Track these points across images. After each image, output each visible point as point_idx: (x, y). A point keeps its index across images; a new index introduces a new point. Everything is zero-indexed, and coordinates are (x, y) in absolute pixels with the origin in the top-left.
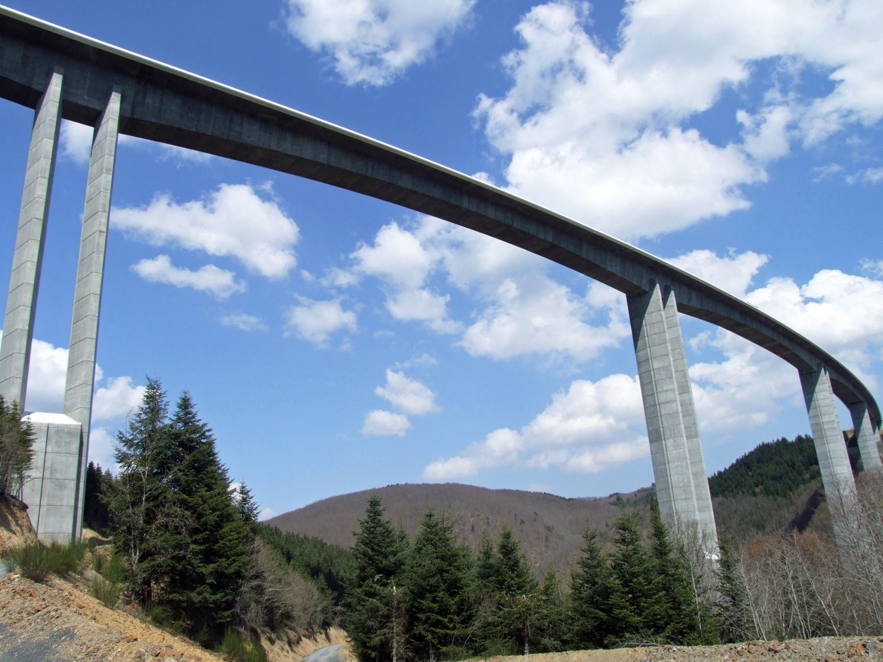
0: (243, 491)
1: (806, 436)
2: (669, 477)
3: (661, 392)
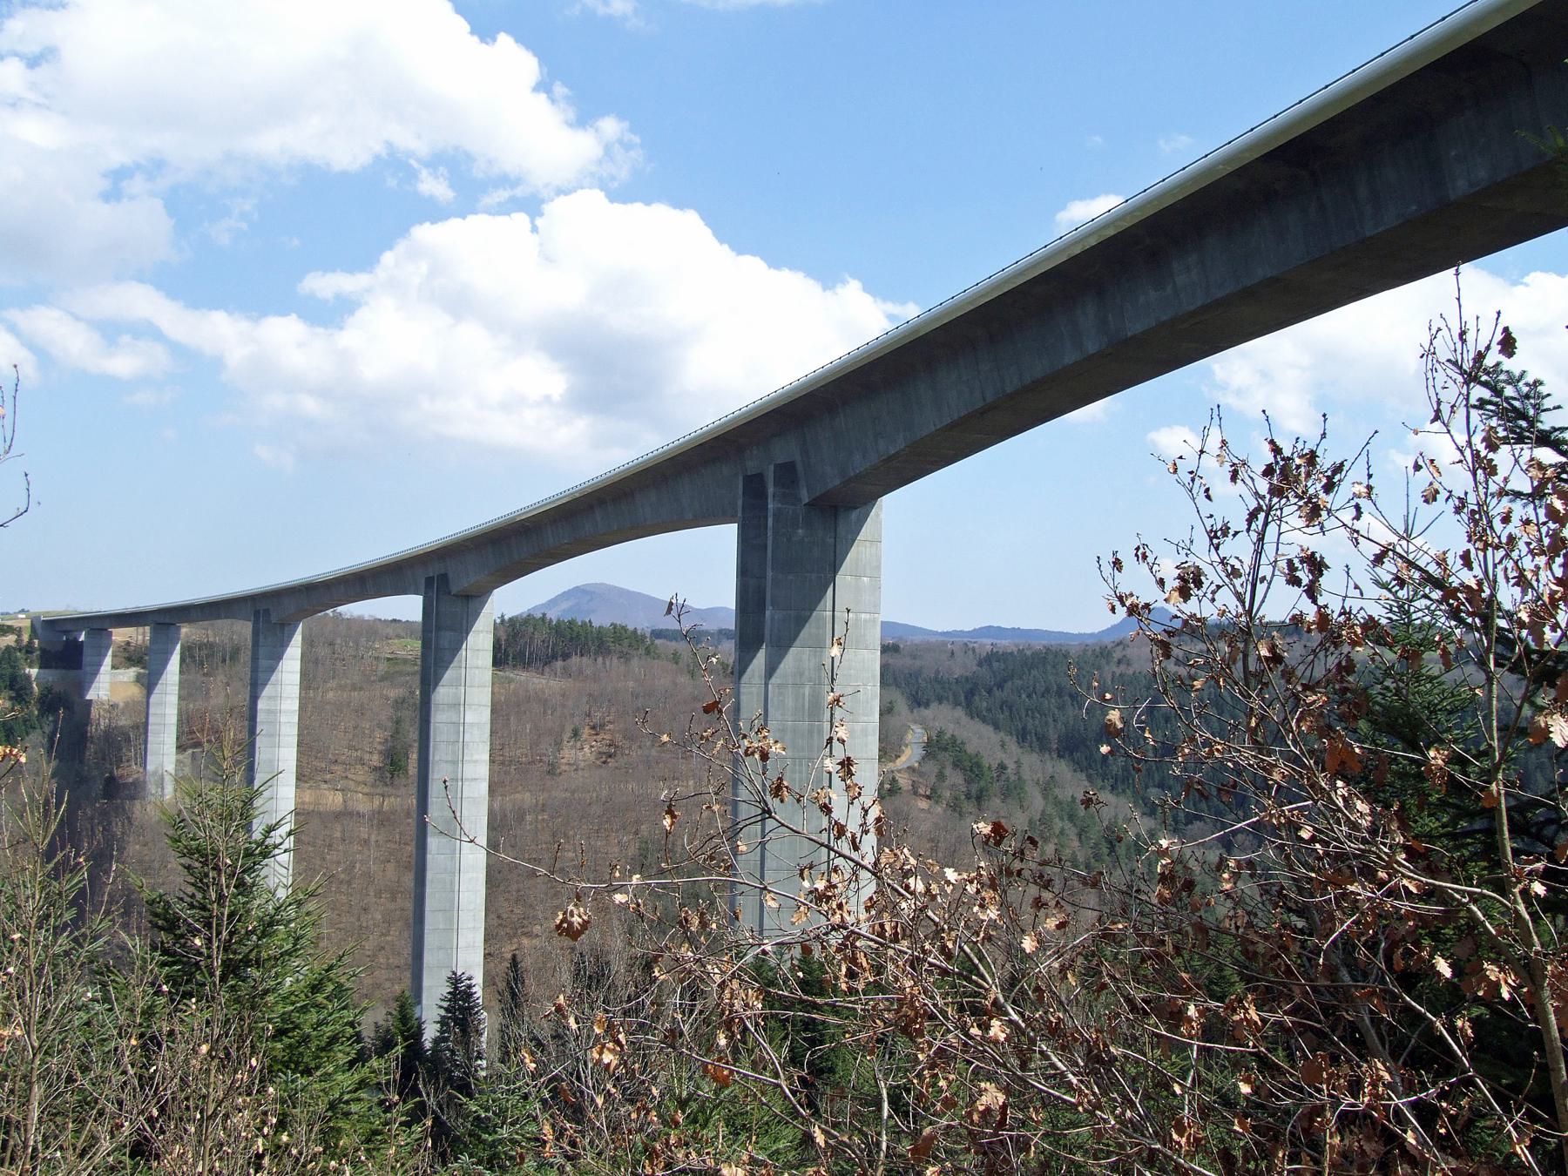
0: (1321, 557)
1: (1496, 465)
2: (456, 894)
3: (469, 762)
